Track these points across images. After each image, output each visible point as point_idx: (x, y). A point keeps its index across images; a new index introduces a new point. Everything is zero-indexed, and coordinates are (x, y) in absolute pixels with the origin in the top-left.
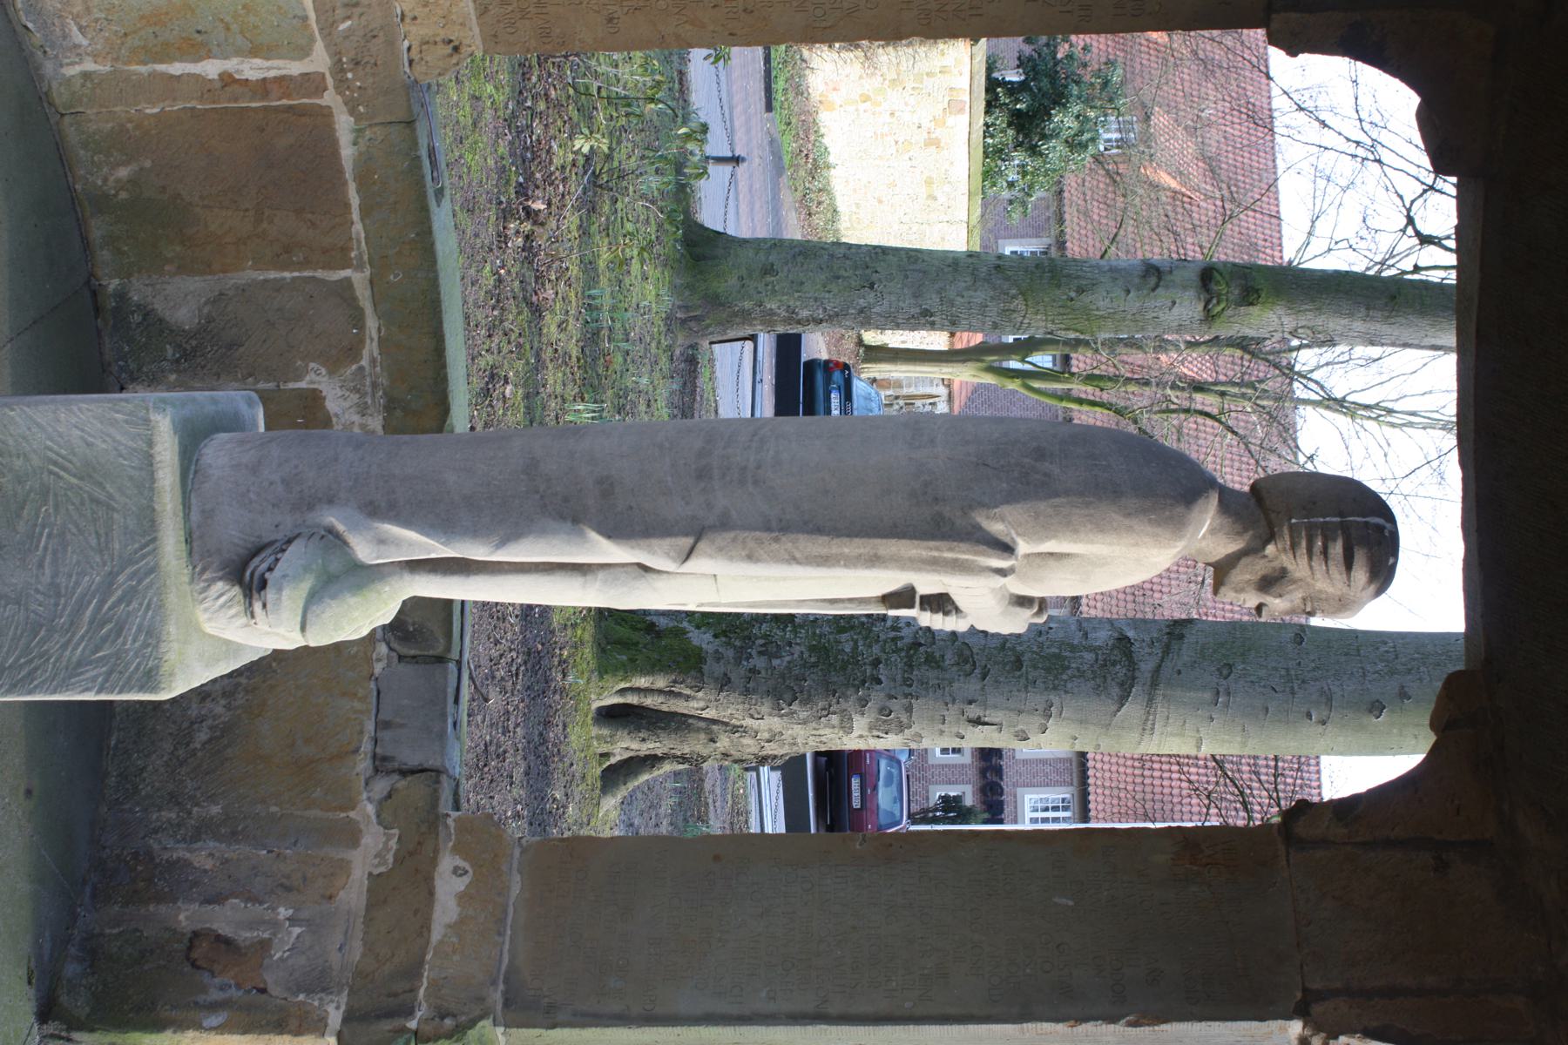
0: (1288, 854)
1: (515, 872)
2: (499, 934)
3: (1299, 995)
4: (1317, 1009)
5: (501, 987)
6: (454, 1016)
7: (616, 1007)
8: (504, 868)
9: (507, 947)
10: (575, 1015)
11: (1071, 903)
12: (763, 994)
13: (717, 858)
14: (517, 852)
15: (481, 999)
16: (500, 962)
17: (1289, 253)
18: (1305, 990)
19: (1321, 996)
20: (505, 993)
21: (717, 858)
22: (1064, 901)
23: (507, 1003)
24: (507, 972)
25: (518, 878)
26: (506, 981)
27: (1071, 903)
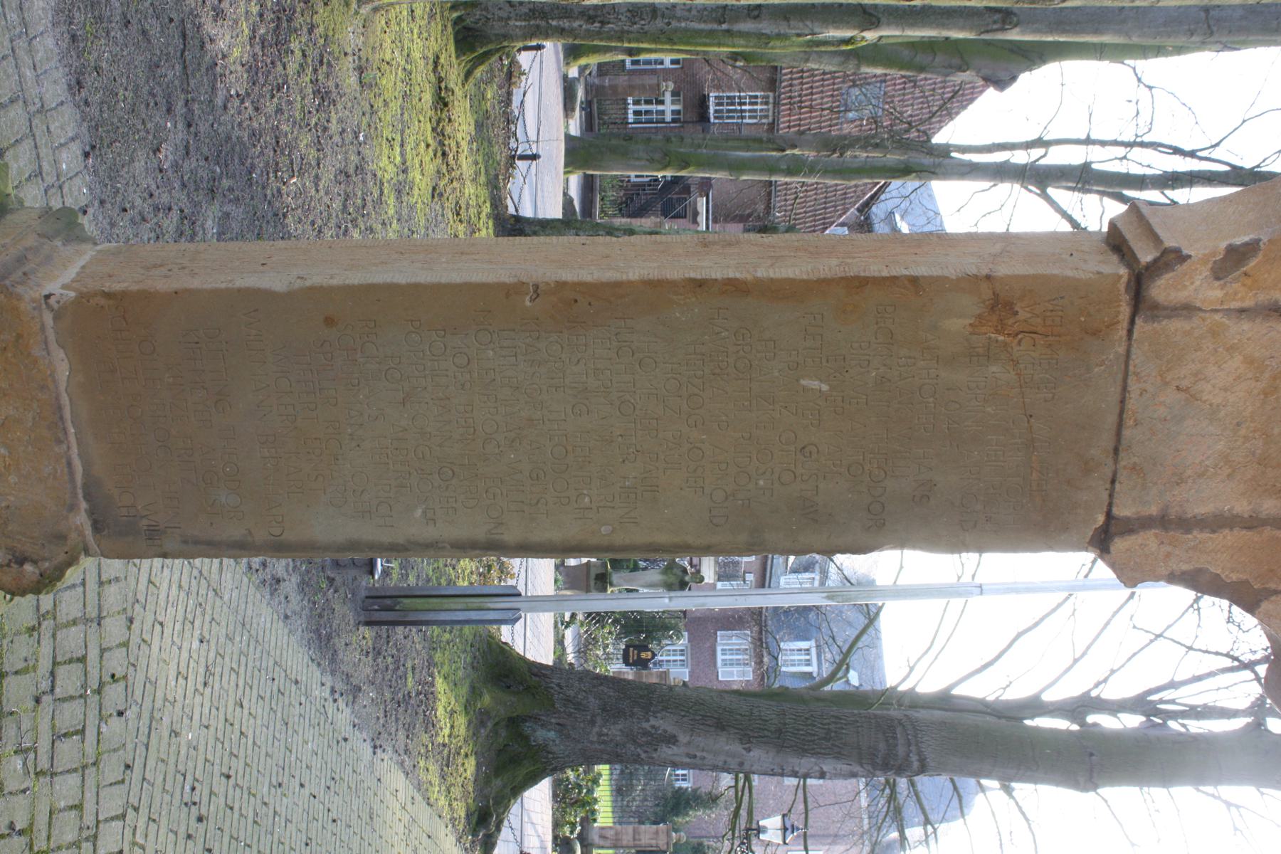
0: (1132, 322)
1: (53, 346)
2: (59, 442)
3: (1101, 519)
4: (1119, 545)
5: (84, 505)
6: (35, 562)
7: (235, 532)
8: (37, 352)
9: (75, 450)
10: (185, 542)
11: (825, 388)
12: (419, 513)
13: (329, 321)
14: (48, 318)
15: (61, 538)
16: (71, 473)
17: (890, 682)
18: (1109, 515)
19: (1130, 527)
20: (91, 513)
21: (329, 321)
22: (815, 384)
23: (97, 527)
24: (86, 486)
25: (59, 355)
26: (88, 497)
27: (825, 388)
